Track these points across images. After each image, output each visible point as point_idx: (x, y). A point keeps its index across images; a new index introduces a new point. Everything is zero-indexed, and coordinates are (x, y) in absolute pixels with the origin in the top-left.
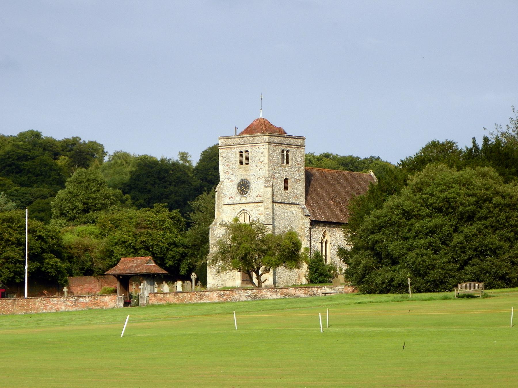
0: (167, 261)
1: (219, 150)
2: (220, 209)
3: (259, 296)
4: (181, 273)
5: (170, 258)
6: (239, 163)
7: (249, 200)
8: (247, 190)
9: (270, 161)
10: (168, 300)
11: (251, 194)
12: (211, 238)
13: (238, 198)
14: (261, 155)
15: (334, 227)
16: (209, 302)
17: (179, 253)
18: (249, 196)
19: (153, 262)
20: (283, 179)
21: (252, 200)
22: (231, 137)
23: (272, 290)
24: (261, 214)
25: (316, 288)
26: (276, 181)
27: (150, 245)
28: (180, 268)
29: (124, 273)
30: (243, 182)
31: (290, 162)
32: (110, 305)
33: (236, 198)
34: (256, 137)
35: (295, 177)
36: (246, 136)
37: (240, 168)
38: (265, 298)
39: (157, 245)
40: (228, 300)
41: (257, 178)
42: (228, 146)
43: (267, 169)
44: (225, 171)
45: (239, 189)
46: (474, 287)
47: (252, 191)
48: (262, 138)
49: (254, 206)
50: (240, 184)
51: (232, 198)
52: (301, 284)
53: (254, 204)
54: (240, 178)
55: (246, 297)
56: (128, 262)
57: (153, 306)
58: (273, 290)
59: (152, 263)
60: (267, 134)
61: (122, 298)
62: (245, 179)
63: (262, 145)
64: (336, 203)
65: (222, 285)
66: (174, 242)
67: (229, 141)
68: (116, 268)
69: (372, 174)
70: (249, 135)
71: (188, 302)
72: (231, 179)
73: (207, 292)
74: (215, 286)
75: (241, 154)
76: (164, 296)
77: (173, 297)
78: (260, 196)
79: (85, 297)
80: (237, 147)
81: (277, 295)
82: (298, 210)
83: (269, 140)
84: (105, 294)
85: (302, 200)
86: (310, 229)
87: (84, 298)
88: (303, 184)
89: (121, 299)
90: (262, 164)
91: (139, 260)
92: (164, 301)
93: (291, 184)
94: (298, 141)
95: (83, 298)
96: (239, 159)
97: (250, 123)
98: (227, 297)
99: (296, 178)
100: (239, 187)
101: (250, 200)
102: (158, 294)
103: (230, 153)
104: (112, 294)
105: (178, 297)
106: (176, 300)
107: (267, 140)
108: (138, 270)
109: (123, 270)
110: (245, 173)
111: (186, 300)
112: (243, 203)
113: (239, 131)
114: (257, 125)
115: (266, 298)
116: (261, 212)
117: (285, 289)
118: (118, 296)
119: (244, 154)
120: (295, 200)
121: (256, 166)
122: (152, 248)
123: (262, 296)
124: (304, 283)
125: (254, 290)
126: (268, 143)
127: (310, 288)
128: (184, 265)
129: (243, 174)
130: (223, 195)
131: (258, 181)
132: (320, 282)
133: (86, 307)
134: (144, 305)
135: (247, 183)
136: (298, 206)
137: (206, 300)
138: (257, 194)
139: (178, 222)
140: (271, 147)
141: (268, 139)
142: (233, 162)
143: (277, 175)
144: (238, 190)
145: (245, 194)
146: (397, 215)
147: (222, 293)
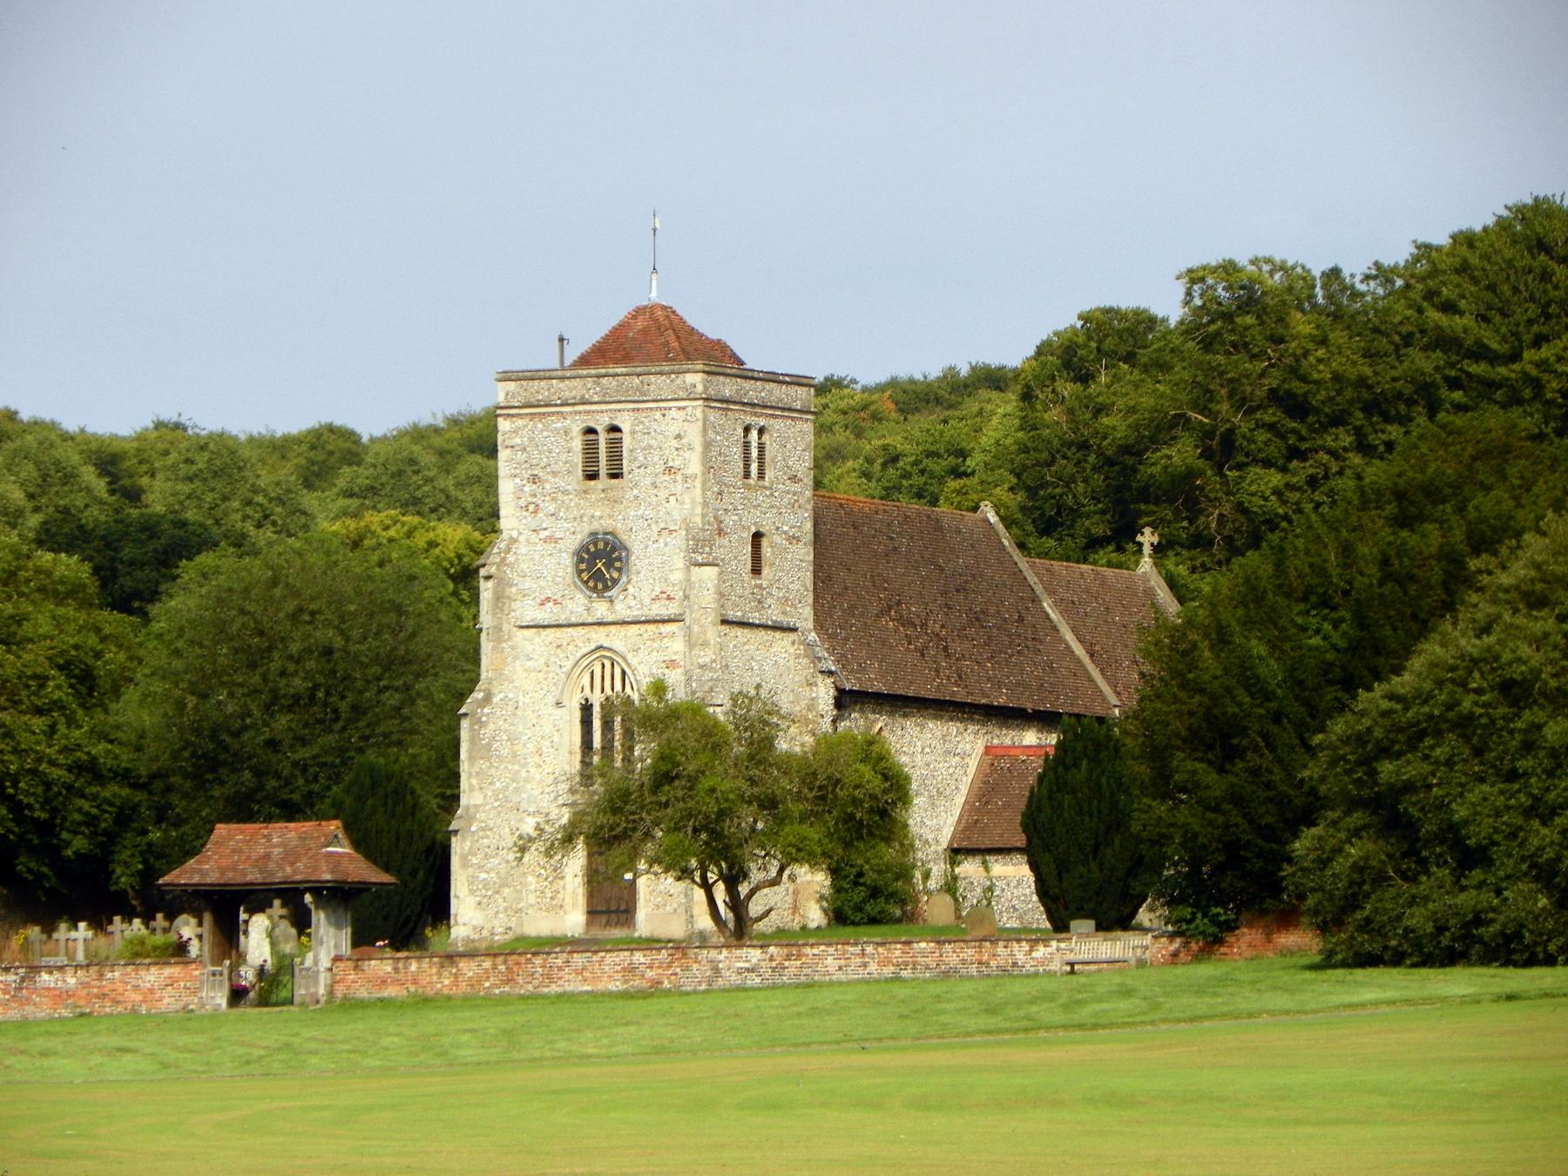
0: (65, 835)
1: (500, 420)
2: (504, 645)
4: (116, 883)
5: (79, 824)
6: (580, 473)
7: (622, 610)
8: (615, 575)
9: (708, 468)
10: (415, 982)
11: (631, 590)
12: (470, 751)
13: (578, 604)
14: (675, 443)
15: (905, 716)
16: (587, 992)
17: (111, 804)
18: (621, 597)
19: (346, 842)
20: (747, 536)
21: (635, 613)
22: (548, 374)
23: (846, 947)
24: (671, 664)
25: (1024, 944)
26: (726, 542)
27: (8, 774)
28: (112, 866)
29: (239, 880)
30: (601, 545)
31: (769, 474)
32: (166, 1001)
33: (570, 605)
35: (786, 528)
36: (611, 371)
37: (585, 492)
38: (816, 978)
39: (34, 772)
40: (666, 984)
41: (655, 528)
42: (534, 408)
43: (699, 499)
44: (522, 502)
45: (582, 571)
46: (223, 871)
47: (635, 579)
48: (679, 382)
50: (588, 551)
51: (551, 604)
52: (804, 928)
53: (643, 628)
54: (586, 529)
55: (739, 972)
56: (244, 841)
57: (352, 1005)
58: (851, 949)
59: (341, 846)
60: (700, 367)
61: (221, 975)
64: (903, 625)
65: (510, 928)
66: (94, 760)
67: (541, 390)
68: (199, 862)
69: (993, 517)
72: (546, 533)
74: (485, 933)
75: (592, 437)
76: (396, 970)
77: (434, 970)
78: (669, 598)
79: (61, 968)
80: (576, 413)
81: (865, 965)
82: (792, 650)
83: (706, 388)
84: (147, 961)
85: (804, 615)
86: (834, 721)
87: (57, 975)
88: (808, 554)
89: (218, 978)
90: (679, 477)
92: (398, 988)
93: (773, 553)
94: (794, 394)
95: (51, 973)
96: (580, 456)
97: (615, 322)
98: (660, 971)
99: (785, 533)
100: (581, 560)
102: (373, 962)
103: (545, 434)
104: (176, 959)
105: (454, 971)
106: (447, 982)
107: (700, 388)
108: (295, 873)
109: (234, 869)
111: (487, 984)
112: (600, 624)
113: (572, 354)
114: (645, 331)
115: (823, 978)
117: (899, 946)
118: (205, 966)
119: (603, 438)
120: (784, 613)
121: (654, 486)
122: (15, 785)
123: (805, 971)
124: (813, 925)
125: (772, 949)
127: (1001, 944)
128: (129, 852)
129: (598, 514)
130: (514, 590)
131: (661, 541)
132: (873, 921)
133: (66, 1007)
135: (614, 549)
136: (792, 636)
137: (573, 985)
139: (81, 684)
140: (713, 416)
141: (705, 386)
143: (730, 520)
144: (580, 572)
145: (607, 588)
146: (1479, 691)
147: (639, 957)
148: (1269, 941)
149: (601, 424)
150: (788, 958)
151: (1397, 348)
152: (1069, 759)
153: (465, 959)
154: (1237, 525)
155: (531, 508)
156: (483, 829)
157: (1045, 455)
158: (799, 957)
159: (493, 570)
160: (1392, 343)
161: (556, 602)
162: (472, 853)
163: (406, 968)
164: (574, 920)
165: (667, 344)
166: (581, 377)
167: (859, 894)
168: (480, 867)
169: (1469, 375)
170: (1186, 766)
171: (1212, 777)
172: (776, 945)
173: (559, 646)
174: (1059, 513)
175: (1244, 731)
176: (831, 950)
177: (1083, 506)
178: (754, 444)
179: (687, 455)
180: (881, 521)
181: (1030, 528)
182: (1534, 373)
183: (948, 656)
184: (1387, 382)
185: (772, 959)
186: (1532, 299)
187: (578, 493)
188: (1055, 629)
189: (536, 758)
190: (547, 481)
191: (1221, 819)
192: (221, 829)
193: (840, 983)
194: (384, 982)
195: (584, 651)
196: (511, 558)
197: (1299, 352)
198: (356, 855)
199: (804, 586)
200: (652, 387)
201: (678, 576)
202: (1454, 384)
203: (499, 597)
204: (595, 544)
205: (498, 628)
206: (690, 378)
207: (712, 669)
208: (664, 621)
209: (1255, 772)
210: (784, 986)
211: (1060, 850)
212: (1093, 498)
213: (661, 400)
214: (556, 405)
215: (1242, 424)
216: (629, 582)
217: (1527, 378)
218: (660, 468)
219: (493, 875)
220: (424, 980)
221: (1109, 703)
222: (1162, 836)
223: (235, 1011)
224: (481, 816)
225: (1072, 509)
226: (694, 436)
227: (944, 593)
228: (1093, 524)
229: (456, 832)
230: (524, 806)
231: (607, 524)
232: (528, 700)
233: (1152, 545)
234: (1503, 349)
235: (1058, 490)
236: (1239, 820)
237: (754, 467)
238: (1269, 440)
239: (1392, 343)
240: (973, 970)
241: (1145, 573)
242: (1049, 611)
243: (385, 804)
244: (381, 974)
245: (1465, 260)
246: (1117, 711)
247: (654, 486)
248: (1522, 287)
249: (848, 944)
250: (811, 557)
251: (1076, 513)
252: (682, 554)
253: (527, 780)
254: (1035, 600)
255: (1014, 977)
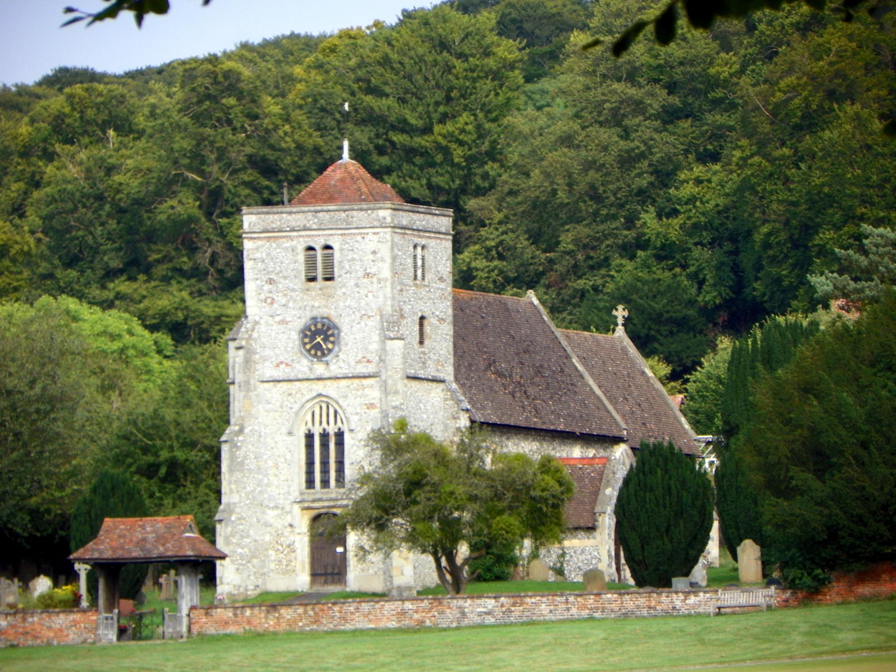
3: (517, 614)
6: (303, 278)
7: (335, 368)
8: (330, 346)
9: (395, 273)
10: (249, 623)
11: (341, 355)
13: (304, 365)
14: (371, 257)
16: (372, 629)
18: (334, 361)
19: (195, 529)
20: (417, 319)
25: (680, 594)
29: (127, 555)
30: (319, 326)
31: (428, 276)
32: (71, 636)
34: (355, 213)
36: (325, 208)
38: (534, 618)
40: (428, 623)
41: (358, 315)
43: (389, 295)
44: (262, 297)
46: (114, 549)
47: (344, 348)
49: (352, 387)
55: (480, 614)
56: (126, 529)
57: (204, 638)
58: (558, 599)
59: (193, 532)
60: (389, 206)
61: (112, 618)
62: (323, 318)
63: (374, 233)
65: (258, 586)
68: (95, 544)
69: (536, 302)
70: (335, 208)
71: (308, 629)
73: (363, 604)
74: (242, 590)
75: (311, 252)
76: (235, 615)
77: (263, 615)
78: (369, 361)
80: (300, 236)
81: (568, 609)
83: (393, 220)
84: (57, 610)
85: (448, 372)
89: (110, 621)
90: (375, 280)
91: (160, 525)
92: (237, 627)
96: (303, 266)
98: (423, 614)
99: (437, 316)
100: (306, 336)
101: (340, 371)
102: (219, 610)
106: (272, 623)
107: (389, 220)
110: (323, 302)
111: (301, 624)
112: (319, 379)
114: (342, 180)
116: (372, 402)
117: (592, 597)
118: (100, 613)
119: (319, 253)
120: (438, 370)
121: (357, 285)
125: (502, 599)
126: (389, 230)
129: (317, 304)
130: (257, 356)
134: (182, 637)
135: (329, 329)
136: (442, 386)
137: (361, 623)
138: (360, 356)
140: (397, 238)
142: (285, 274)
143: (407, 308)
144: (305, 344)
145: (324, 355)
148: (851, 591)
149: (318, 244)
150: (514, 605)
151: (339, 122)
152: (647, 468)
153: (284, 608)
154: (228, 259)
155: (269, 301)
156: (239, 519)
157: (70, 205)
158: (521, 604)
159: (244, 343)
160: (334, 119)
161: (287, 365)
162: (233, 535)
163: (242, 613)
164: (302, 580)
165: (359, 189)
166: (303, 212)
167: (489, 560)
168: (238, 545)
169: (393, 144)
170: (802, 476)
171: (816, 484)
172: (505, 597)
173: (290, 395)
174: (81, 251)
175: (841, 453)
176: (544, 599)
177: (101, 245)
178: (419, 257)
179: (380, 264)
180: (475, 306)
181: (56, 262)
182: (444, 142)
183: (528, 397)
184: (334, 150)
185: (502, 606)
186: (438, 86)
187: (302, 291)
188: (582, 377)
189: (274, 471)
190: (280, 282)
191: (826, 512)
192: (108, 522)
193: (553, 622)
194: (227, 623)
195: (308, 397)
196: (255, 335)
197: (270, 127)
198: (202, 538)
199: (448, 352)
200: (355, 219)
201: (375, 346)
202: (381, 151)
203: (247, 361)
204: (315, 325)
205: (247, 383)
206: (382, 213)
207: (401, 409)
208: (365, 377)
209: (849, 480)
210: (511, 624)
211: (643, 530)
212: (109, 239)
213: (362, 228)
214: (286, 231)
215: (229, 182)
216: (340, 350)
217: (440, 148)
218: (360, 274)
219: (246, 550)
220: (256, 621)
221: (620, 427)
222: (785, 521)
223: (122, 643)
224: (238, 510)
225: (91, 248)
226: (385, 251)
227: (518, 354)
228: (110, 259)
229: (220, 521)
230: (266, 502)
231: (324, 312)
232: (268, 431)
233: (624, 317)
234: (420, 123)
235: (80, 233)
236: (838, 511)
237: (419, 272)
238: (249, 195)
239: (334, 119)
240: (645, 612)
241: (620, 337)
242: (577, 365)
243: (122, 501)
244: (225, 618)
245: (387, 55)
246: (625, 432)
247: (357, 285)
248: (431, 78)
249: (556, 595)
250: (452, 333)
251: (95, 250)
252: (378, 332)
253: (268, 485)
254: (568, 357)
255: (675, 617)
